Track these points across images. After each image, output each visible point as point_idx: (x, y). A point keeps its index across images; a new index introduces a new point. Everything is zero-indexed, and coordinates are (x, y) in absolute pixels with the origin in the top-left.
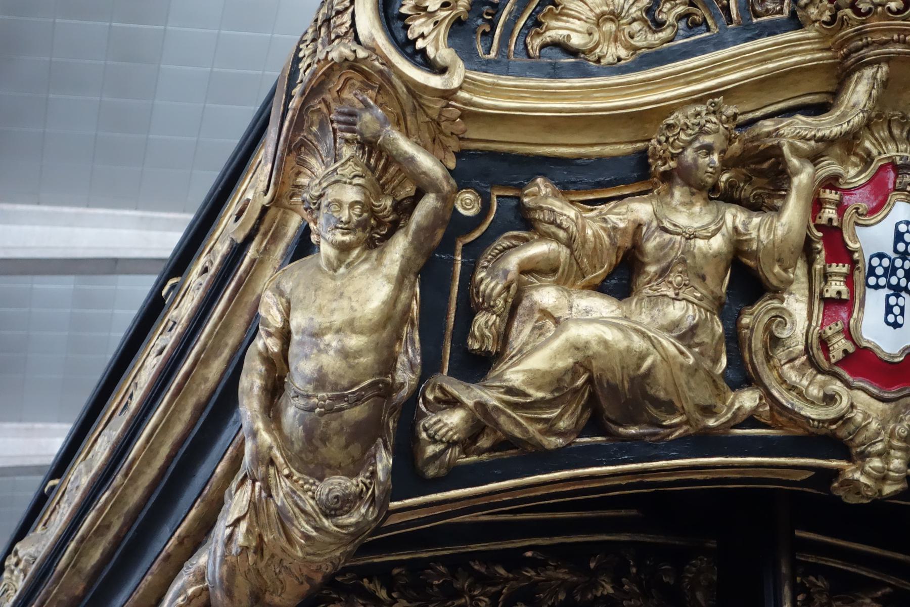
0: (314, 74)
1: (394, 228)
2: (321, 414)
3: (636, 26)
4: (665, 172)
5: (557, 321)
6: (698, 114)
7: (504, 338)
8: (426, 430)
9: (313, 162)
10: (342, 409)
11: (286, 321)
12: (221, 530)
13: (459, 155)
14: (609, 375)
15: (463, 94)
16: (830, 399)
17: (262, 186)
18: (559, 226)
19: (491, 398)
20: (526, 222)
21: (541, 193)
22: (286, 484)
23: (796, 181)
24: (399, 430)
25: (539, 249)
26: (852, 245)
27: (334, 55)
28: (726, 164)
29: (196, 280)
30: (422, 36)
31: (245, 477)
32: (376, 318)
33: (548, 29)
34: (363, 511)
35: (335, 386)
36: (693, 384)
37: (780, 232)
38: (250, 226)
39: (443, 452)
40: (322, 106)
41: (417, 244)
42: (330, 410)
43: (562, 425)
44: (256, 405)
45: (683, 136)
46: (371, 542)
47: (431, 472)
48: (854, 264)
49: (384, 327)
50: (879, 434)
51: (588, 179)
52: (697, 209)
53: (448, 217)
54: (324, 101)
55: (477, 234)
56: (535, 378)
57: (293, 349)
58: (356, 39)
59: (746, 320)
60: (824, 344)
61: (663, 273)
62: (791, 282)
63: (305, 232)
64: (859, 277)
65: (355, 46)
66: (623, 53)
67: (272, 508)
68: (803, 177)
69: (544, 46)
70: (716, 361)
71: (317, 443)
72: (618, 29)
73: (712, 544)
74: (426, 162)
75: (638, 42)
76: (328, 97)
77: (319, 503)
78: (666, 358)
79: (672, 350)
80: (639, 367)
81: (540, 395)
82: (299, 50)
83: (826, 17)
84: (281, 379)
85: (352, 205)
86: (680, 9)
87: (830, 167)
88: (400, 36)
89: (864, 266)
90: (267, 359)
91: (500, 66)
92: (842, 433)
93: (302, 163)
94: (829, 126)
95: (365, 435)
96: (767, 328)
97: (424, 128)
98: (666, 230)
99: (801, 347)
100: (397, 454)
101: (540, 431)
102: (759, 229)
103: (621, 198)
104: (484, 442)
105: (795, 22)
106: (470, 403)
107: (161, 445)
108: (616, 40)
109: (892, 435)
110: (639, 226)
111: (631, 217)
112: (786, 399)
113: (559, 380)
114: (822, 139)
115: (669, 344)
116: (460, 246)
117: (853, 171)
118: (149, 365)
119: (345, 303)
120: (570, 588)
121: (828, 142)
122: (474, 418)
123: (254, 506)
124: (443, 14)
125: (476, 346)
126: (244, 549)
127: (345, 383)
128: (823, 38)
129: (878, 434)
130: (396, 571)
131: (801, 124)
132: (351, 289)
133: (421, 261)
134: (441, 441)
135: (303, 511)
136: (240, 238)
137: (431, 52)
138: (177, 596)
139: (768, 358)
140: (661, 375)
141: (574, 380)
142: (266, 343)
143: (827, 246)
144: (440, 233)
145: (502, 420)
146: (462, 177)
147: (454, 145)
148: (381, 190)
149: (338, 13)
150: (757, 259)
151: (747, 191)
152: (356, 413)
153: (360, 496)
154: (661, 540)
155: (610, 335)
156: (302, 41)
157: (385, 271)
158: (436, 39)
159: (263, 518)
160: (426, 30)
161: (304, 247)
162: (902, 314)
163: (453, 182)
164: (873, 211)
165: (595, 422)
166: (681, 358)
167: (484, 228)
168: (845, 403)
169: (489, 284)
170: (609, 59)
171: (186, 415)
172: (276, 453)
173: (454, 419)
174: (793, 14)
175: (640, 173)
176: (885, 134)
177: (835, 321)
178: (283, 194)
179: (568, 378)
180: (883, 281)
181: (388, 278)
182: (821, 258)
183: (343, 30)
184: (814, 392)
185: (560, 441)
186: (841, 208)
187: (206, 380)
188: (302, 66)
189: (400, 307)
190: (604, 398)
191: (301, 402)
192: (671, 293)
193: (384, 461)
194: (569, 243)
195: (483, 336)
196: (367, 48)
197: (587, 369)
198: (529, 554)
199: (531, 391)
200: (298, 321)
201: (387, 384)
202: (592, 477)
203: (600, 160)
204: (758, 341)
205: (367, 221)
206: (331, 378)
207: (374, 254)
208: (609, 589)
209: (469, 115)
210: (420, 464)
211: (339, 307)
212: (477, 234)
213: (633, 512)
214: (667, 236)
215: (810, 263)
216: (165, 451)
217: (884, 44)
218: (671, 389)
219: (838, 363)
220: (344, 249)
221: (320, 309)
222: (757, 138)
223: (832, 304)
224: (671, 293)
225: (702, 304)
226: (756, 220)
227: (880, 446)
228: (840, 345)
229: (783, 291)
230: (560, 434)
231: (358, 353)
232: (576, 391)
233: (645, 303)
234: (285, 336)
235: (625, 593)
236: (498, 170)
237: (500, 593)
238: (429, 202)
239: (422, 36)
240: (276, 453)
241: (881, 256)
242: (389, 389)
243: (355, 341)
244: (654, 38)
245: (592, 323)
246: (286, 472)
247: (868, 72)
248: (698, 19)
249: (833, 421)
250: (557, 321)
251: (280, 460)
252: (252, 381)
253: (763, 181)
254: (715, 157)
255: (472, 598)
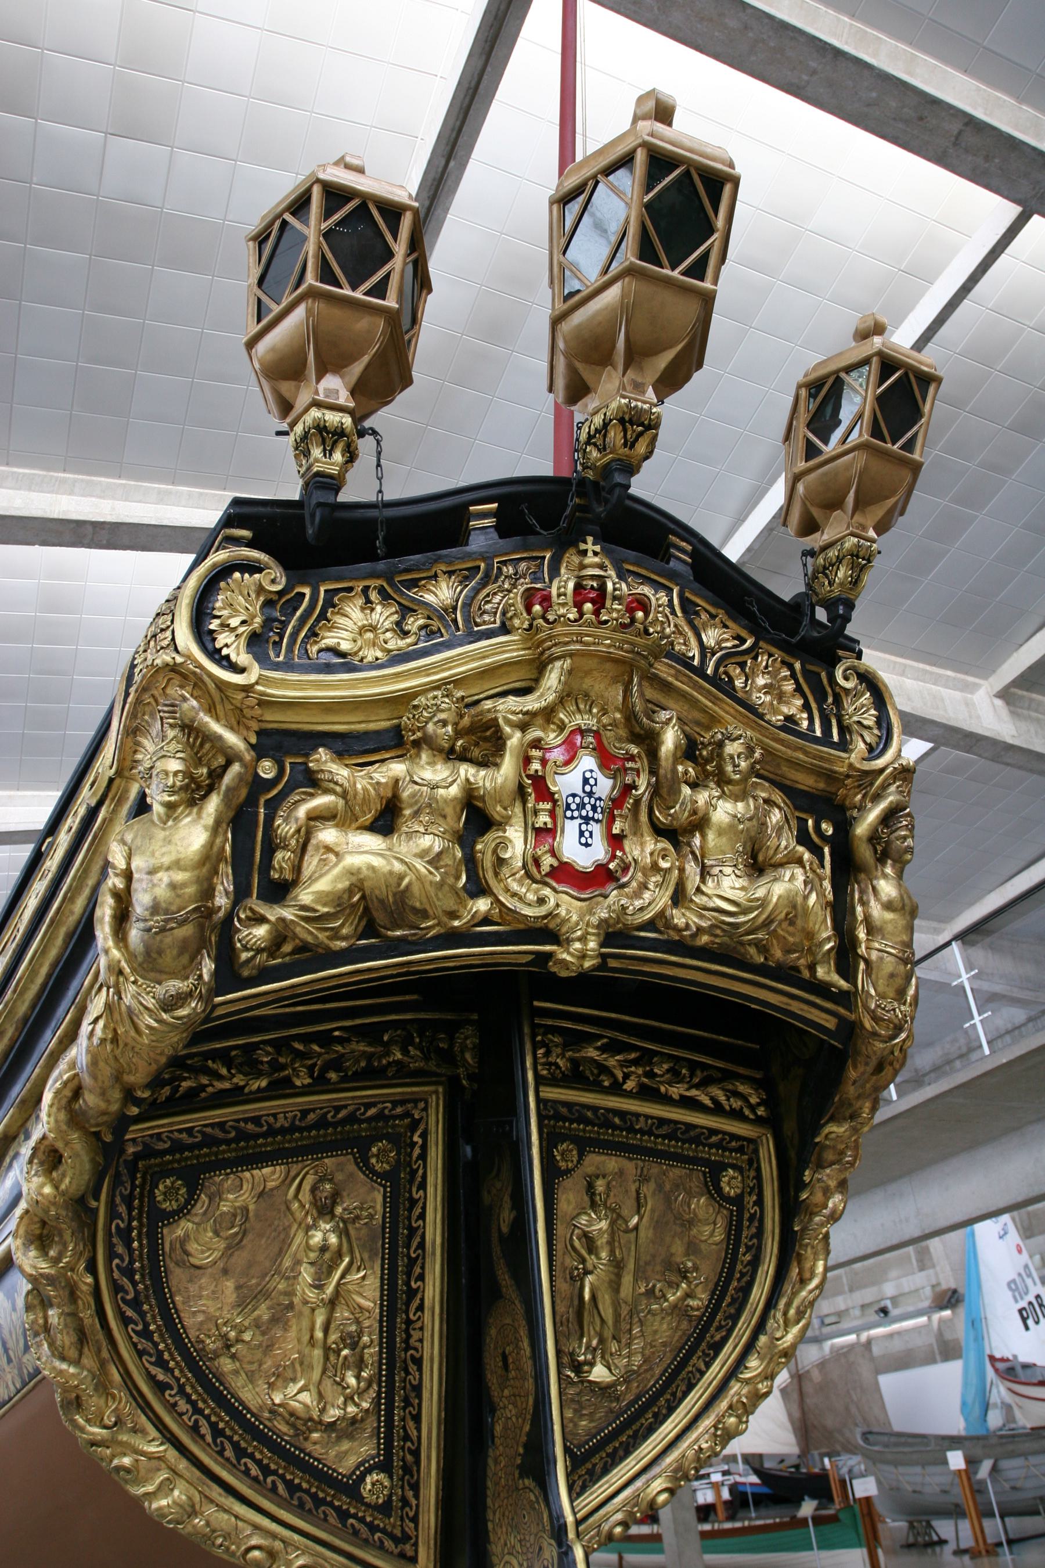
0: (144, 677)
1: (210, 789)
2: (156, 933)
3: (389, 635)
4: (414, 741)
5: (337, 854)
6: (435, 697)
7: (298, 869)
8: (240, 941)
9: (146, 743)
10: (172, 929)
11: (129, 864)
12: (85, 1028)
13: (259, 733)
14: (377, 892)
15: (259, 688)
16: (541, 901)
17: (108, 762)
18: (336, 783)
19: (288, 914)
20: (312, 781)
21: (323, 759)
22: (132, 988)
23: (509, 743)
24: (219, 943)
25: (322, 800)
26: (553, 789)
27: (158, 662)
28: (458, 734)
29: (64, 839)
30: (227, 646)
31: (101, 986)
32: (197, 858)
33: (323, 638)
34: (193, 1005)
35: (167, 912)
36: (440, 895)
37: (499, 781)
38: (100, 793)
39: (253, 957)
40: (151, 700)
41: (227, 800)
42: (163, 930)
43: (344, 931)
44: (107, 929)
45: (425, 714)
46: (205, 1032)
47: (246, 973)
48: (555, 802)
49: (204, 864)
50: (578, 924)
51: (353, 747)
52: (439, 767)
53: (250, 779)
54: (153, 696)
55: (275, 792)
56: (321, 897)
57: (135, 885)
58: (176, 650)
59: (479, 847)
60: (537, 862)
61: (416, 814)
62: (510, 817)
63: (143, 796)
64: (559, 811)
65: (174, 655)
66: (379, 654)
67: (123, 1008)
68: (515, 740)
69: (320, 651)
70: (458, 878)
71: (154, 955)
72: (376, 636)
73: (475, 1017)
74: (232, 739)
75: (390, 646)
76: (155, 693)
77: (158, 1001)
78: (419, 878)
79: (423, 870)
80: (399, 885)
81: (326, 910)
82: (134, 659)
83: (526, 625)
84: (127, 908)
85: (176, 774)
86: (421, 622)
87: (535, 733)
88: (210, 647)
89: (562, 803)
90: (116, 895)
91: (288, 666)
92: (552, 926)
93: (138, 744)
94: (532, 703)
95: (191, 952)
96: (495, 851)
97: (230, 713)
98: (416, 783)
99: (520, 864)
100: (217, 960)
101: (328, 938)
102: (481, 778)
103: (383, 761)
104: (287, 948)
105: (505, 630)
106: (272, 918)
107: (41, 966)
108: (374, 645)
109: (588, 925)
110: (397, 781)
111: (391, 774)
112: (509, 902)
113: (340, 898)
114: (527, 713)
115: (420, 866)
116: (262, 801)
117: (552, 735)
118: (31, 902)
119: (172, 848)
120: (370, 1057)
121: (532, 715)
122: (277, 931)
123: (108, 1006)
124: (241, 629)
125: (276, 876)
126: (103, 1041)
127: (174, 908)
128: (524, 640)
129: (578, 924)
130: (233, 1053)
131: (512, 702)
132: (177, 837)
133: (231, 814)
134: (252, 949)
135: (146, 1008)
136: (93, 803)
137: (233, 657)
138: (56, 1081)
139: (496, 874)
140: (416, 889)
141: (351, 897)
142: (115, 881)
143: (535, 790)
144: (244, 793)
145: (298, 930)
146: (260, 751)
147: (255, 726)
148: (199, 762)
149: (162, 630)
150: (484, 802)
151: (476, 753)
152: (187, 931)
153: (190, 994)
154: (436, 1016)
155: (377, 862)
156: (137, 652)
157: (202, 822)
158: (238, 647)
159: (117, 1016)
160: (229, 641)
161: (142, 807)
162: (591, 836)
163: (253, 753)
164: (567, 763)
165: (370, 929)
166: (431, 877)
167: (280, 787)
168: (552, 903)
169: (286, 828)
170: (370, 659)
171: (59, 941)
172: (123, 964)
173: (261, 931)
174: (503, 624)
175: (395, 742)
176: (574, 708)
177: (544, 844)
178: (124, 768)
179: (346, 896)
180: (576, 814)
181: (205, 827)
182: (531, 799)
183: (166, 643)
184: (531, 897)
185: (344, 944)
186: (544, 762)
187: (72, 913)
188: (137, 670)
189: (215, 849)
190: (375, 911)
191: (141, 925)
192: (422, 830)
193: (208, 967)
194: (344, 795)
195: (281, 868)
196: (182, 655)
197: (361, 889)
198: (337, 1033)
199: (319, 908)
200: (137, 863)
201: (208, 908)
202: (370, 970)
203: (366, 733)
204: (488, 861)
205: (187, 786)
206: (164, 905)
207: (195, 810)
208: (399, 1056)
209: (265, 703)
210: (236, 967)
211: (169, 852)
212: (275, 792)
213: (415, 997)
214: (417, 787)
215: (524, 802)
216: (44, 970)
217: (567, 643)
218: (425, 900)
219: (547, 875)
220: (170, 807)
221: (153, 854)
222: (481, 713)
223: (542, 833)
224: (422, 830)
225: (446, 836)
226: (482, 773)
227: (579, 933)
228: (548, 861)
229: (506, 824)
230: (344, 938)
231: (184, 885)
232: (354, 906)
233: (403, 837)
234: (128, 875)
235: (412, 1057)
236: (288, 744)
237: (315, 1065)
238: (236, 768)
239: (227, 646)
240: (123, 964)
241: (574, 795)
242: (212, 911)
243: (180, 876)
244: (401, 643)
245: (364, 852)
246: (132, 979)
247: (558, 664)
248: (435, 628)
249: (545, 917)
250: (337, 854)
251: (127, 970)
252: (106, 911)
253: (488, 745)
254: (449, 728)
255: (294, 1069)
